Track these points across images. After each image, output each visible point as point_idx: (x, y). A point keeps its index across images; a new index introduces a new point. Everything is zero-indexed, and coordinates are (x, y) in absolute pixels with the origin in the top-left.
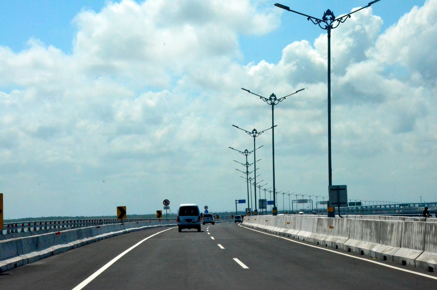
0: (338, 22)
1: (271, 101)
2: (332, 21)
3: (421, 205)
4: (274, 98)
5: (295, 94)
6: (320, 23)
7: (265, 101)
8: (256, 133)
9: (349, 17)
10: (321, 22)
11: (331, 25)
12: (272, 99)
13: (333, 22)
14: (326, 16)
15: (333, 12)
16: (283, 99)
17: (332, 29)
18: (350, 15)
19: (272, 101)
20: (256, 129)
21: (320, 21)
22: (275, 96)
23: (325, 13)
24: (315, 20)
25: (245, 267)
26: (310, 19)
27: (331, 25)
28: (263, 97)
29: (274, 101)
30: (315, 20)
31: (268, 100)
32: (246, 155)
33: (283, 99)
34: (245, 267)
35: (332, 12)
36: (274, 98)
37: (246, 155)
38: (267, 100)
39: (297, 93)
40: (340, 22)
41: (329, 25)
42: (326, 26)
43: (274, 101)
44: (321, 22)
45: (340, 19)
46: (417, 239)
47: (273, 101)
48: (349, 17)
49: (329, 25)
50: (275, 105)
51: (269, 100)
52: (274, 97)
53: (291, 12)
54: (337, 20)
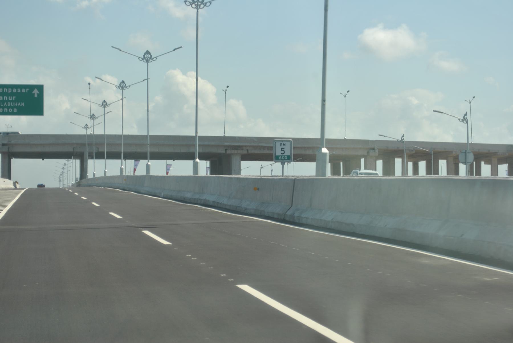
53: (122, 52)
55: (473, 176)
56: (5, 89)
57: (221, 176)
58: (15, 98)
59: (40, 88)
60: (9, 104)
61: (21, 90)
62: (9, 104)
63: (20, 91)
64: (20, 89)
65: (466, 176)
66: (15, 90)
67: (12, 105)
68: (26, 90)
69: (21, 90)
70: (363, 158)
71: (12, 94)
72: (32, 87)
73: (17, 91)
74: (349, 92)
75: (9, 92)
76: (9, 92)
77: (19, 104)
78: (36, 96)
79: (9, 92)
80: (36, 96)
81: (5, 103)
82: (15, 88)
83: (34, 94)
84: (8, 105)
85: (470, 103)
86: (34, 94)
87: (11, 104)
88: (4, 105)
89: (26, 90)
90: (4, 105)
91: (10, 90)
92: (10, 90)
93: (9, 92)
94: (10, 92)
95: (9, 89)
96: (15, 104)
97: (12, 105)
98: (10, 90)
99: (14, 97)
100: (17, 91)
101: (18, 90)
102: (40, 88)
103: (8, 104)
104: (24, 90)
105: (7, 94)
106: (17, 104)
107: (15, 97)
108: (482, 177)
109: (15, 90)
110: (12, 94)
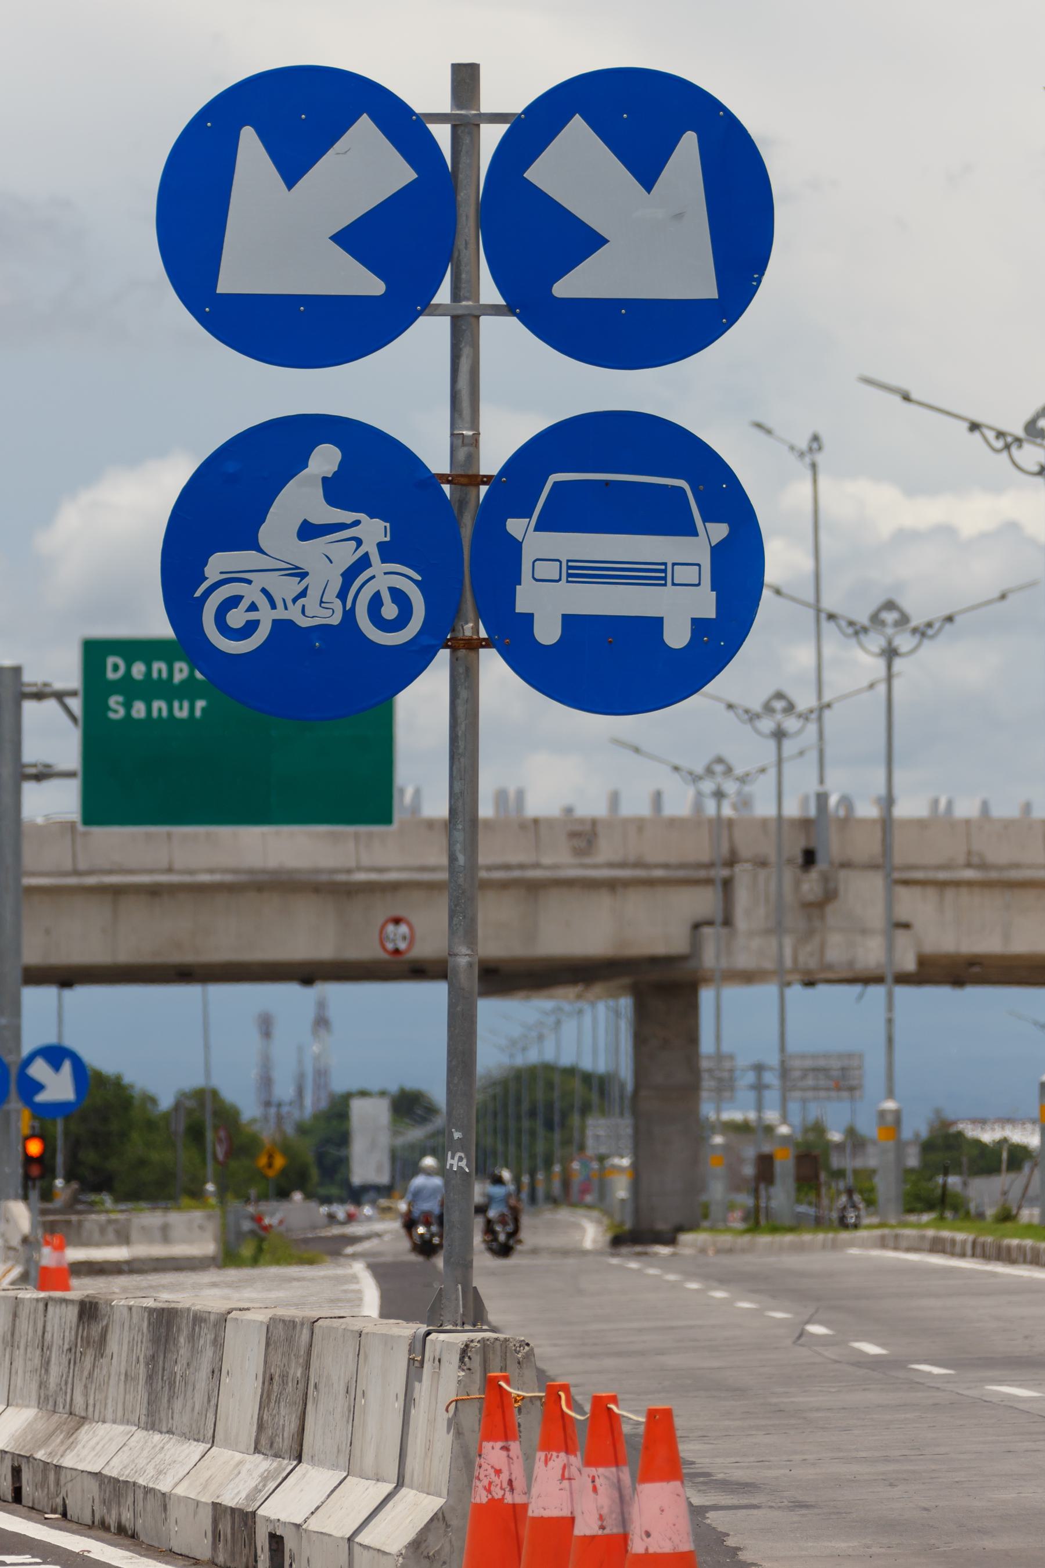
58: (203, 710)
63: (122, 712)
64: (112, 715)
79: (178, 678)
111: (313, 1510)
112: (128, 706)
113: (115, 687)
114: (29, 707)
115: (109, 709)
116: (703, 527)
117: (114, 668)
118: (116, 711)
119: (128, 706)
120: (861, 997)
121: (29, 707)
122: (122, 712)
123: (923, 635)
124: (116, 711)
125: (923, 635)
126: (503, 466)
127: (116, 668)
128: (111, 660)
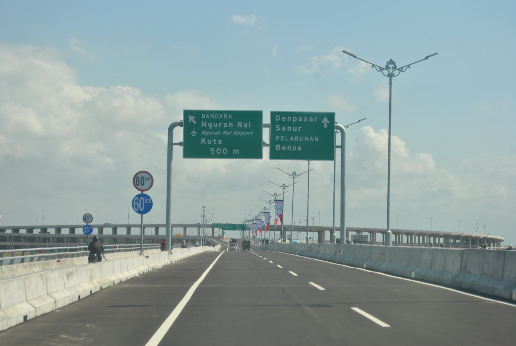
0: (399, 71)
1: (389, 71)
2: (394, 70)
3: (459, 239)
4: (393, 67)
5: (362, 119)
6: (383, 70)
7: (379, 71)
8: (285, 186)
9: (408, 68)
10: (383, 70)
11: (393, 73)
12: (389, 68)
13: (394, 70)
14: (388, 65)
15: (395, 62)
16: (407, 68)
17: (393, 77)
18: (410, 66)
19: (390, 71)
20: (295, 172)
21: (383, 69)
22: (394, 64)
23: (388, 62)
24: (379, 67)
25: (291, 272)
26: (374, 67)
27: (393, 73)
28: (375, 65)
29: (393, 71)
30: (379, 67)
31: (383, 69)
32: (270, 204)
33: (407, 68)
34: (291, 272)
35: (394, 62)
36: (393, 67)
37: (270, 204)
38: (382, 69)
39: (427, 60)
40: (401, 71)
41: (391, 73)
42: (388, 73)
43: (392, 71)
44: (384, 70)
45: (400, 69)
46: (151, 242)
47: (391, 70)
48: (408, 68)
49: (391, 73)
50: (338, 133)
51: (385, 69)
52: (393, 65)
53: (357, 59)
54: (398, 70)
55: (142, 243)
56: (288, 118)
57: (211, 266)
58: (300, 129)
59: (331, 116)
60: (297, 138)
61: (308, 119)
62: (297, 138)
63: (307, 120)
64: (307, 118)
65: (358, 235)
66: (306, 119)
67: (302, 139)
68: (314, 119)
69: (308, 119)
70: (325, 128)
71: (297, 124)
72: (320, 116)
73: (303, 119)
74: (465, 231)
75: (294, 122)
76: (294, 121)
77: (311, 139)
78: (325, 126)
79: (294, 121)
80: (325, 126)
81: (292, 137)
82: (301, 116)
83: (324, 123)
84: (296, 140)
85: (432, 219)
86: (324, 123)
87: (299, 138)
88: (290, 140)
89: (314, 119)
90: (290, 140)
91: (295, 119)
92: (295, 119)
93: (294, 122)
94: (295, 122)
95: (294, 118)
96: (305, 139)
97: (302, 139)
98: (295, 119)
99: (300, 128)
100: (303, 119)
101: (305, 118)
102: (331, 116)
103: (296, 139)
104: (311, 119)
105: (291, 124)
106: (308, 139)
107: (301, 127)
108: (33, 234)
109: (300, 119)
110: (297, 124)
111: (260, 200)
112: (281, 128)
113: (278, 123)
114: (174, 146)
115: (276, 128)
116: (378, 65)
117: (278, 118)
118: (278, 129)
119: (281, 128)
120: (306, 216)
121: (174, 146)
122: (307, 120)
123: (400, 71)
124: (278, 129)
125: (400, 71)
126: (169, 329)
127: (278, 118)
128: (277, 116)
